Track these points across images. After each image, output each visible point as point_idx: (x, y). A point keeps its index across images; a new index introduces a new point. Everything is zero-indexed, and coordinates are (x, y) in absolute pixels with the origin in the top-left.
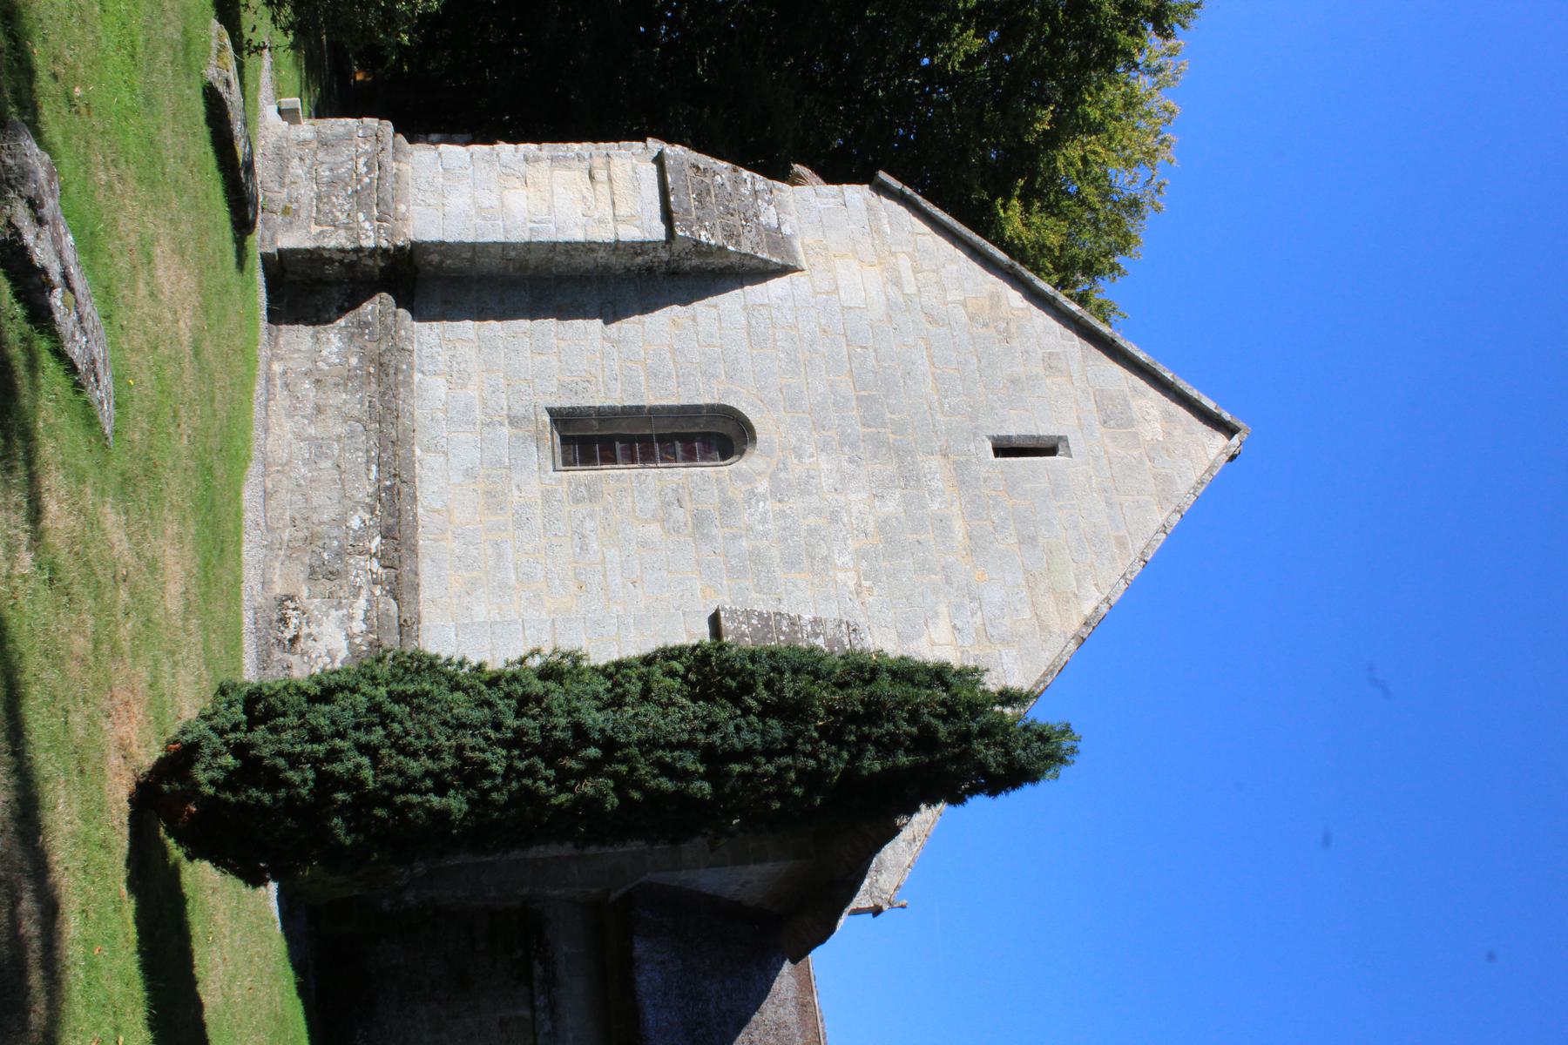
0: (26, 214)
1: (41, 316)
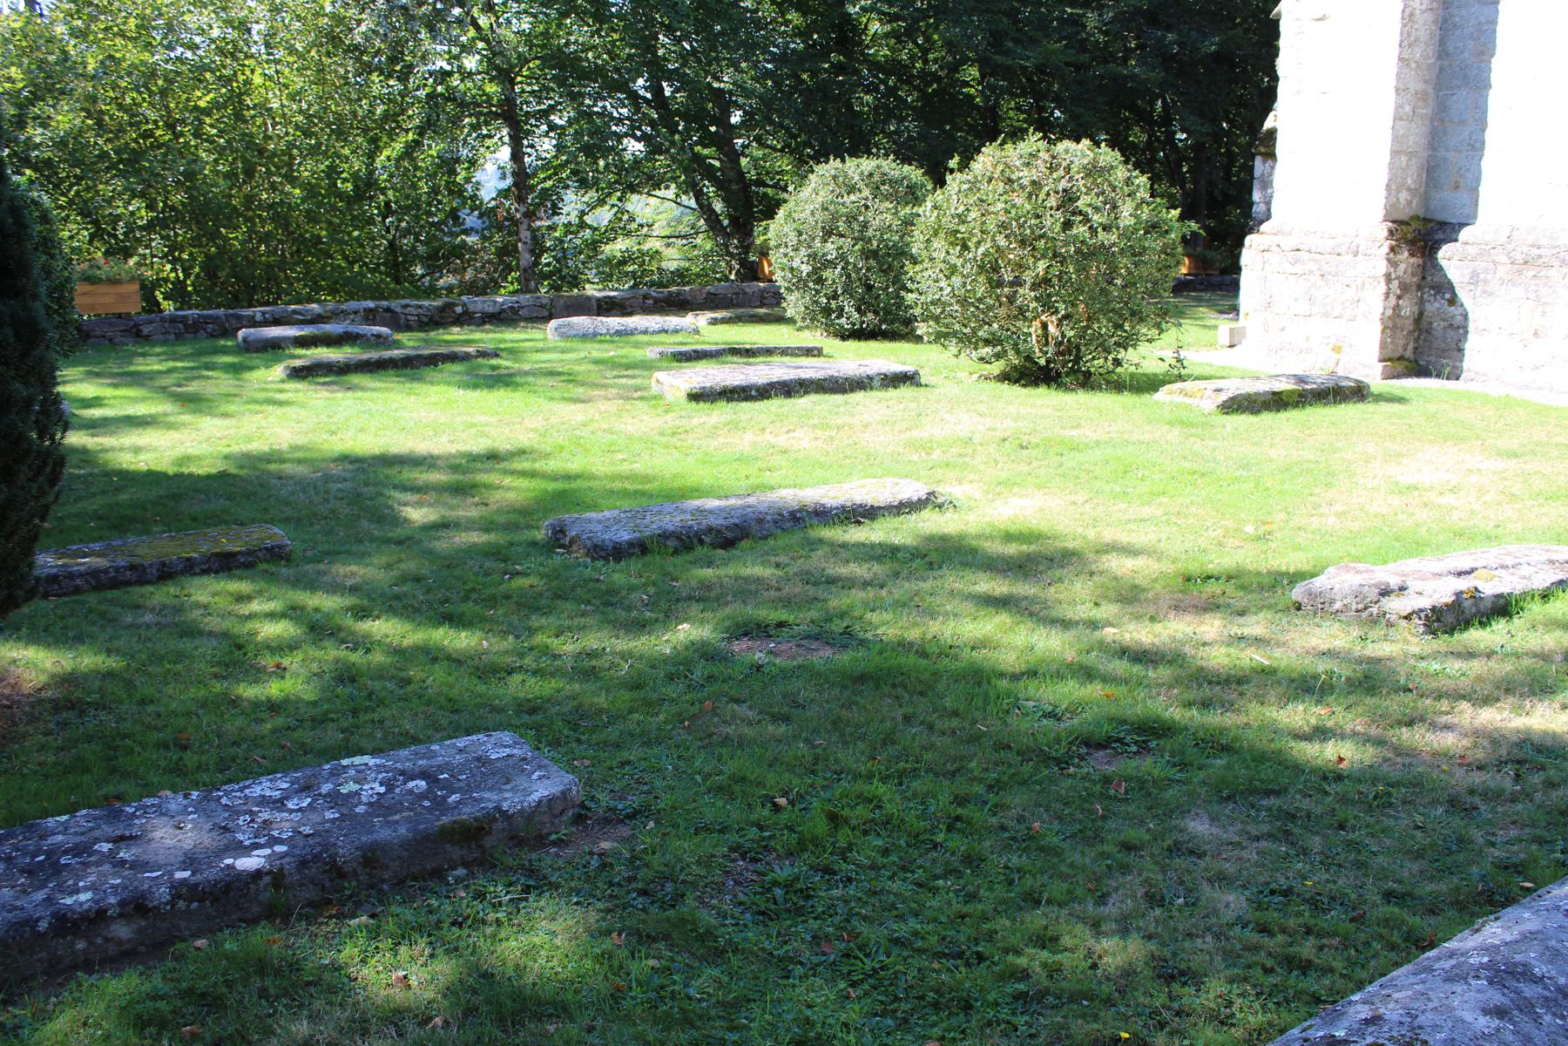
0: (1397, 600)
1: (1503, 608)
